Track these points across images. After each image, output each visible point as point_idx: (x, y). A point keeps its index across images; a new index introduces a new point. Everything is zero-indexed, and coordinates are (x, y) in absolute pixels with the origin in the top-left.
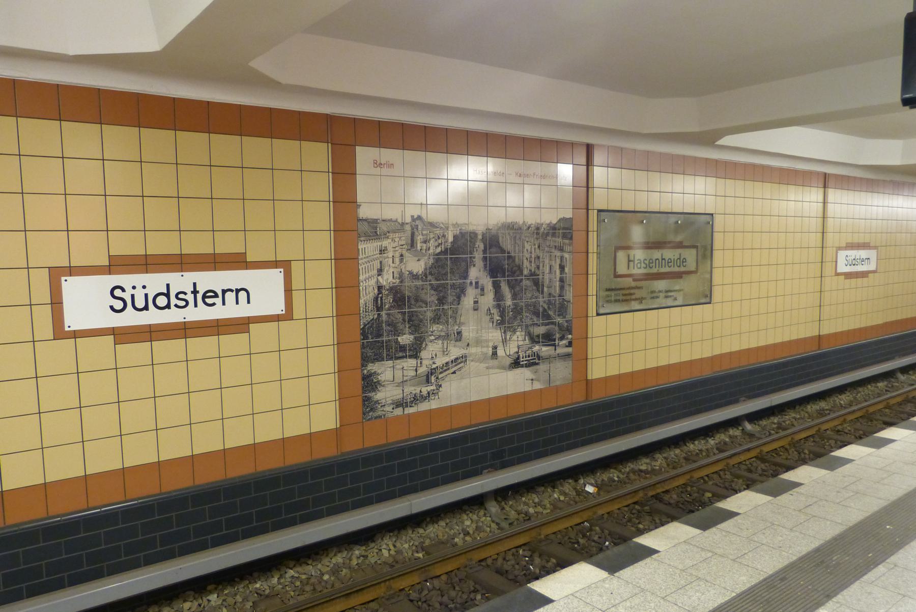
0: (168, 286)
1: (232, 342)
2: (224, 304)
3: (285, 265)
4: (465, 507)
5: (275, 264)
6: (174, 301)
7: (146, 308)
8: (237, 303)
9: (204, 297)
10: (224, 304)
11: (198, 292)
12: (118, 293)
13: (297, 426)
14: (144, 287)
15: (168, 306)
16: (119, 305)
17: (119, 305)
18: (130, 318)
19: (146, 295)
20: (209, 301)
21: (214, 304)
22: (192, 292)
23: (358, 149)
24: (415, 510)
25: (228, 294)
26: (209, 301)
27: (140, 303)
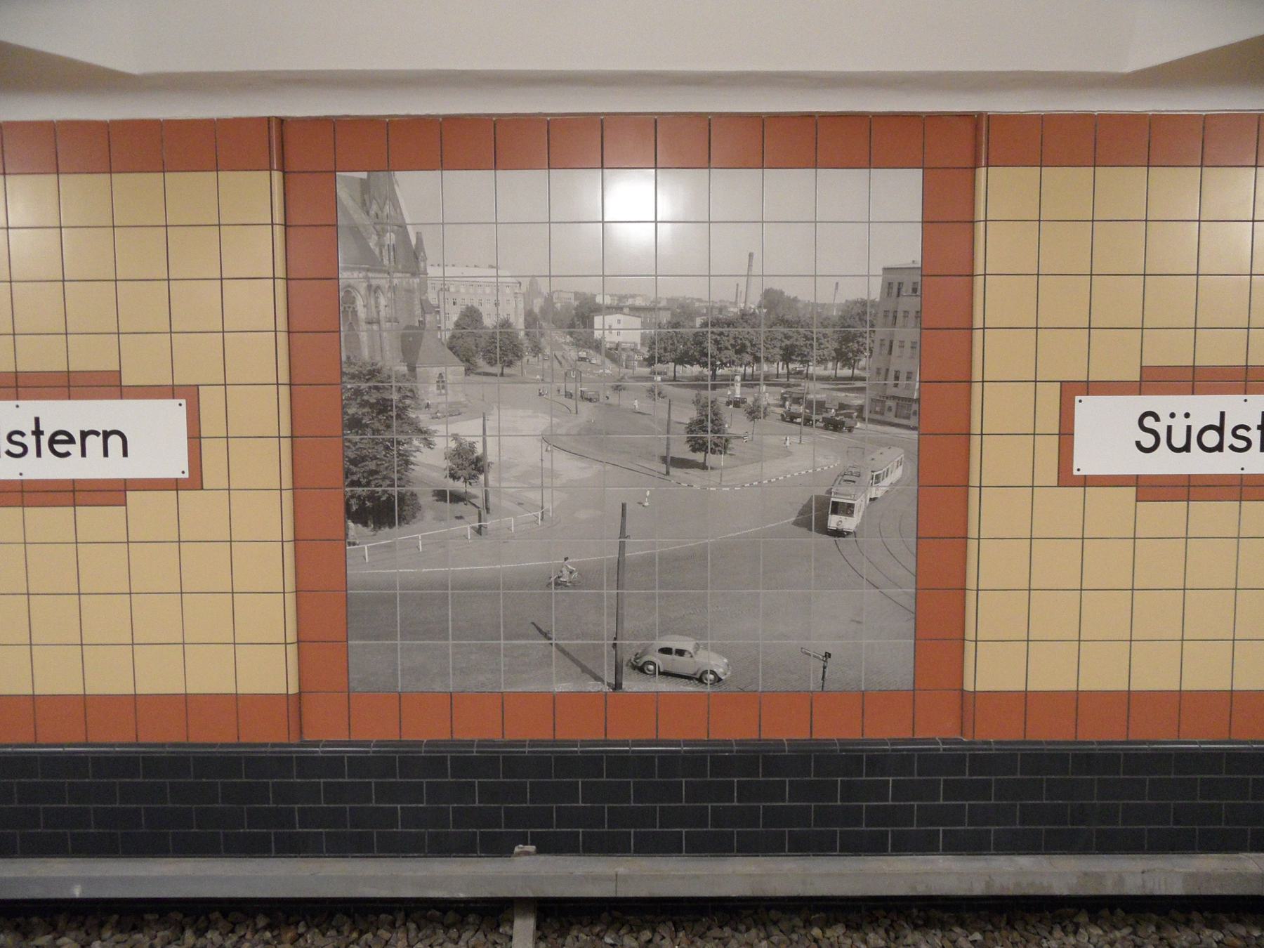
0: (1222, 414)
1: (95, 519)
2: (84, 454)
3: (190, 394)
4: (1195, 916)
5: (171, 391)
6: (1229, 439)
7: (1187, 448)
8: (106, 454)
9: (52, 441)
10: (84, 454)
11: (42, 433)
12: (1149, 422)
13: (210, 676)
14: (1172, 415)
15: (1219, 448)
16: (1148, 440)
17: (1148, 440)
18: (1164, 463)
19: (1189, 428)
20: (60, 448)
21: (68, 454)
22: (33, 433)
23: (916, 176)
24: (1109, 888)
25: (90, 440)
26: (60, 448)
27: (1179, 441)
